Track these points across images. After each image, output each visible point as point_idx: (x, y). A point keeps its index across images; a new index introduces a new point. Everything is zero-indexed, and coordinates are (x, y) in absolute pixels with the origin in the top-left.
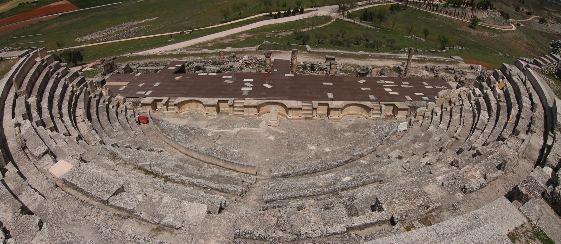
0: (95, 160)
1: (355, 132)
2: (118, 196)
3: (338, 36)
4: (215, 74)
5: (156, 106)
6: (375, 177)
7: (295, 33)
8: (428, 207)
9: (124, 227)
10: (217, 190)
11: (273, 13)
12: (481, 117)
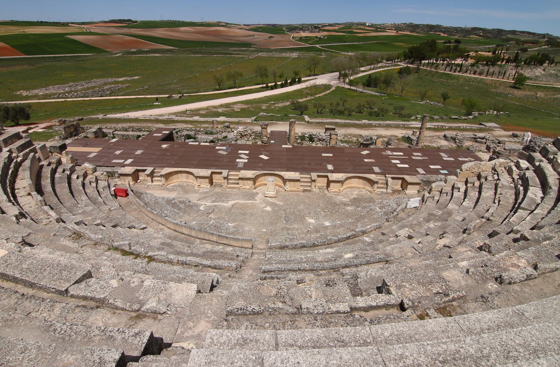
0: (48, 242)
1: (357, 207)
2: (83, 284)
3: (338, 104)
4: (208, 144)
5: (138, 177)
6: (381, 257)
7: (293, 103)
8: (447, 295)
9: (91, 320)
10: (209, 267)
11: (270, 85)
12: (529, 194)
